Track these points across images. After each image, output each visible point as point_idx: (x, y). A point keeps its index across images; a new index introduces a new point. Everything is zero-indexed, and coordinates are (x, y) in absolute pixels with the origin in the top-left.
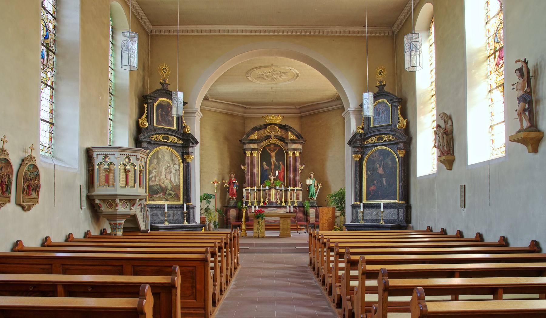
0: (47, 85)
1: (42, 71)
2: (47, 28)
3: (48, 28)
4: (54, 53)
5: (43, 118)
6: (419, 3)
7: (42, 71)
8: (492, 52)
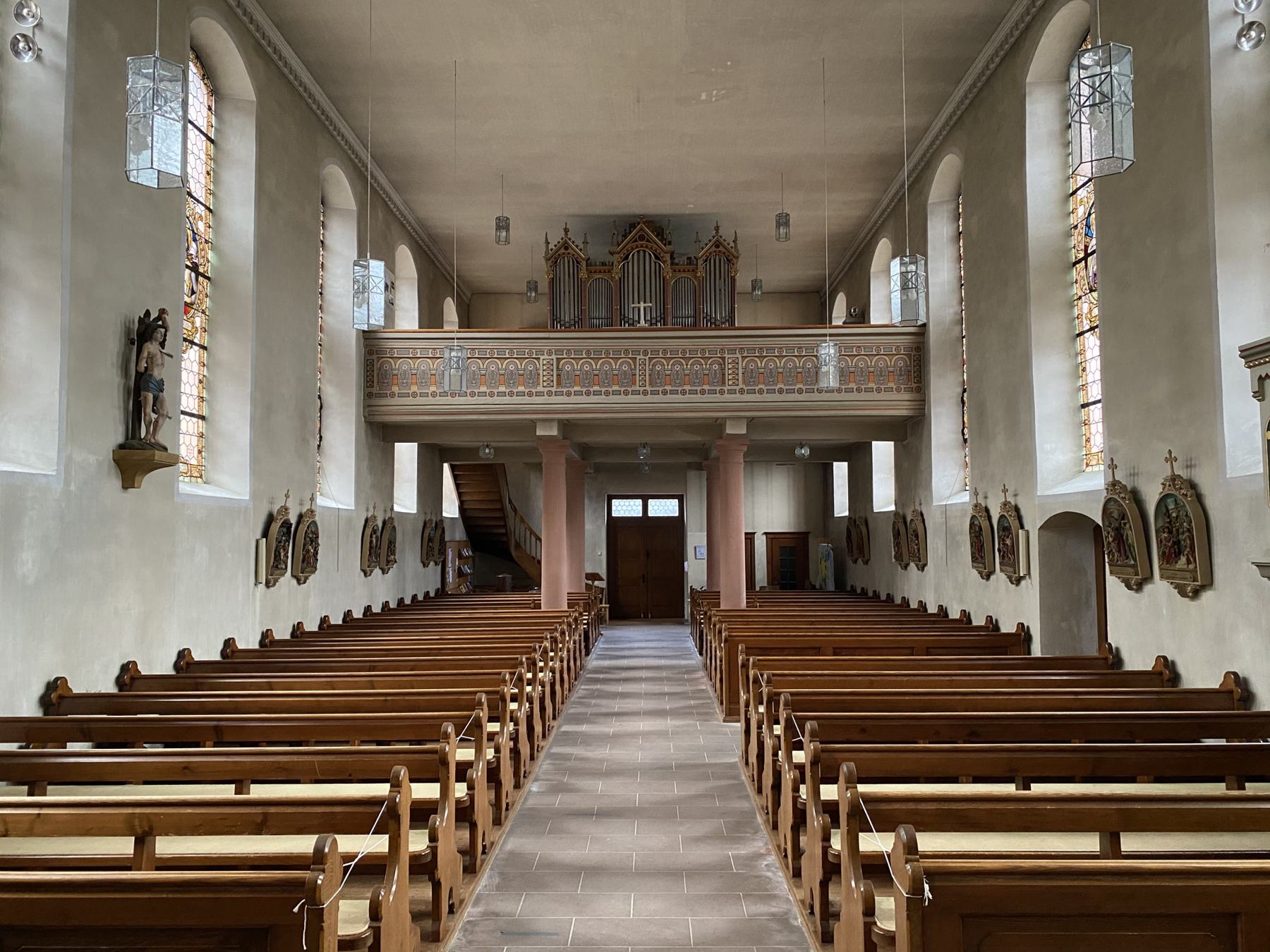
0: (192, 343)
1: (185, 318)
2: (193, 231)
3: (196, 231)
4: (208, 278)
5: (188, 410)
6: (1043, 7)
7: (185, 318)
8: (1082, 255)
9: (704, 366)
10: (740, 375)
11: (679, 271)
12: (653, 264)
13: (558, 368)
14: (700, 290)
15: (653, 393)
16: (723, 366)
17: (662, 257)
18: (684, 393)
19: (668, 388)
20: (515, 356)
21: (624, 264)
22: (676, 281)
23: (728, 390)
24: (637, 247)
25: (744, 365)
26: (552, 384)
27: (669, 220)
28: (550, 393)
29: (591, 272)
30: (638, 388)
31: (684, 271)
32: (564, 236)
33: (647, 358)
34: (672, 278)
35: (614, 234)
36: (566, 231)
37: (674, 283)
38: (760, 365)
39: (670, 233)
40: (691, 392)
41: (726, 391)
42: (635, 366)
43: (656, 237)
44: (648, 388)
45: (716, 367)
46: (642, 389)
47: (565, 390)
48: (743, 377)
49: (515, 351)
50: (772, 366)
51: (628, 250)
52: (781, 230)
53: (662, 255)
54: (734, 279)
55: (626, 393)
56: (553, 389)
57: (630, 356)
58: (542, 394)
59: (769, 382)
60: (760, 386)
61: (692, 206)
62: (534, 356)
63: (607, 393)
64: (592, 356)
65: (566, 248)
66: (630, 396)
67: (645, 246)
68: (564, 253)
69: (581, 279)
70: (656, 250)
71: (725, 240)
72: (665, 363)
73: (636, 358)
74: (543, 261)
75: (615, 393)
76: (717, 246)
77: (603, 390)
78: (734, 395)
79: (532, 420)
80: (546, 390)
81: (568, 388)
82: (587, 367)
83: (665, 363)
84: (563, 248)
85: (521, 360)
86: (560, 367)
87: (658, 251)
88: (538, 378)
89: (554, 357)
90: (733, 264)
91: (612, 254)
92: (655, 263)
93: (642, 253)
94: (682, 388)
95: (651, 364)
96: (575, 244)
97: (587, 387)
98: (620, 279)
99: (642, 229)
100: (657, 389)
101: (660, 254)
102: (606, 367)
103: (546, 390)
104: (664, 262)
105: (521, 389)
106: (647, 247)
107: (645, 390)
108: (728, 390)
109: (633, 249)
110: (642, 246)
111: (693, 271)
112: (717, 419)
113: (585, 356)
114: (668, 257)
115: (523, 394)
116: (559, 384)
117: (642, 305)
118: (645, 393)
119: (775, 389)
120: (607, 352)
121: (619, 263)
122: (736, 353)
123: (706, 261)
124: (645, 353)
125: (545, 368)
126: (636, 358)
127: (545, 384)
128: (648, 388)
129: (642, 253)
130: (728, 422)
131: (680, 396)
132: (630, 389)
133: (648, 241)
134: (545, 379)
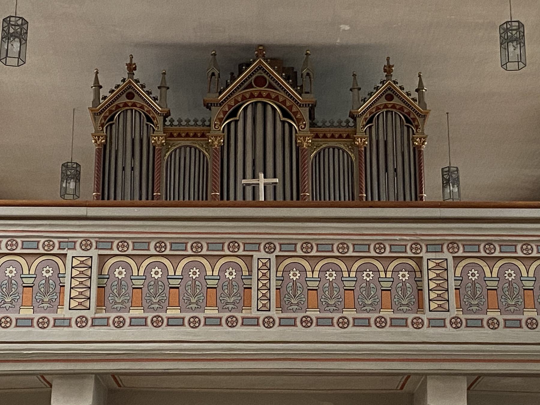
9: (382, 275)
10: (452, 292)
11: (325, 136)
12: (279, 125)
13: (100, 273)
14: (360, 166)
15: (284, 323)
16: (418, 274)
17: (295, 113)
18: (343, 323)
19: (313, 314)
20: (18, 251)
21: (229, 124)
22: (319, 153)
23: (429, 320)
24: (252, 96)
25: (458, 274)
26: (88, 294)
27: (307, 54)
28: (82, 322)
29: (172, 136)
30: (255, 313)
31: (333, 136)
32: (126, 76)
33: (273, 257)
34: (311, 147)
35: (213, 74)
36: (132, 68)
37: (315, 157)
38: (488, 274)
39: (308, 74)
40: (358, 322)
41: (426, 322)
42: (250, 271)
43: (285, 79)
44: (275, 314)
45: (404, 276)
46: (262, 315)
47: (113, 315)
48: (458, 296)
49: (19, 240)
50: (511, 275)
51: (236, 102)
52: (511, 49)
53: (294, 109)
54: (420, 151)
55: (232, 323)
56: (89, 314)
57: (241, 252)
58: (67, 323)
59: (509, 306)
60: (490, 314)
61: (347, 28)
62: (55, 251)
63: (194, 323)
64: (167, 252)
65: (130, 96)
66: (239, 329)
67: (264, 94)
68: (126, 105)
69: (154, 147)
70: (284, 102)
71: (402, 88)
72: (308, 268)
73: (252, 256)
74: (89, 116)
75: (210, 322)
76: (390, 98)
77: (187, 316)
78: (440, 330)
79: (42, 375)
80: (75, 315)
81: (119, 311)
82: (156, 273)
83: (308, 268)
84: (125, 95)
85: (30, 259)
86: (105, 272)
87: (288, 104)
88: (61, 293)
89: (94, 253)
90: (417, 127)
91: (208, 106)
92: (283, 122)
93: (260, 106)
94: (340, 315)
95: (281, 268)
96: (145, 89)
97: (155, 310)
98: (222, 147)
99: (260, 67)
100: (293, 315)
101: (290, 107)
102: (195, 273)
103: (75, 315)
104: (298, 122)
105: (26, 313)
106: (268, 96)
107: (269, 317)
108: (429, 320)
109: (244, 99)
110: (260, 96)
111: (348, 137)
112: (409, 376)
113: (153, 252)
114: (305, 112)
115: (28, 322)
116: (101, 303)
117: (262, 181)
118: (269, 323)
119: (520, 320)
120: (197, 245)
121: (221, 121)
122: (442, 251)
123: (370, 121)
124: (270, 247)
125: (75, 273)
126: (252, 256)
127: (74, 304)
128: (275, 314)
129: (260, 106)
130: (430, 383)
131: (336, 330)
132: (239, 315)
133: (271, 86)
134: (74, 293)
